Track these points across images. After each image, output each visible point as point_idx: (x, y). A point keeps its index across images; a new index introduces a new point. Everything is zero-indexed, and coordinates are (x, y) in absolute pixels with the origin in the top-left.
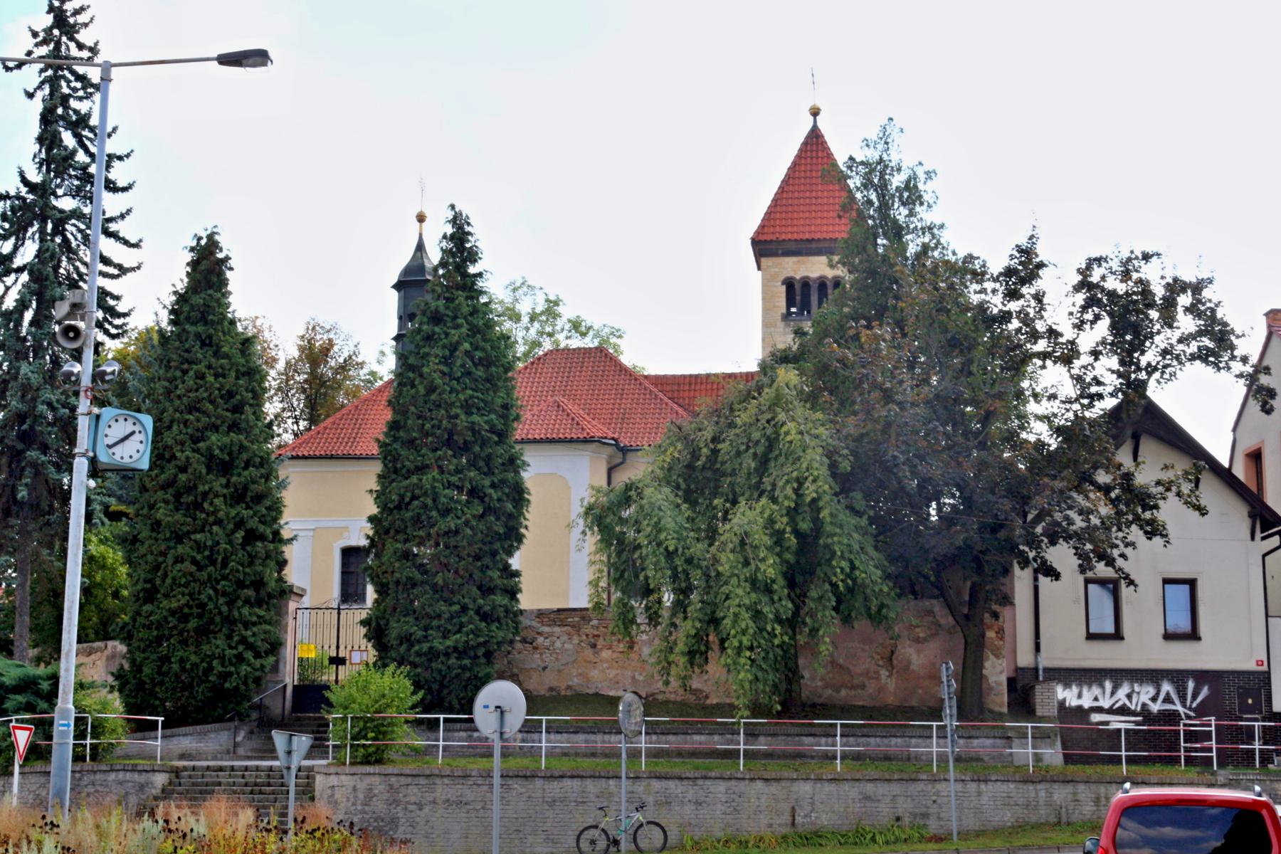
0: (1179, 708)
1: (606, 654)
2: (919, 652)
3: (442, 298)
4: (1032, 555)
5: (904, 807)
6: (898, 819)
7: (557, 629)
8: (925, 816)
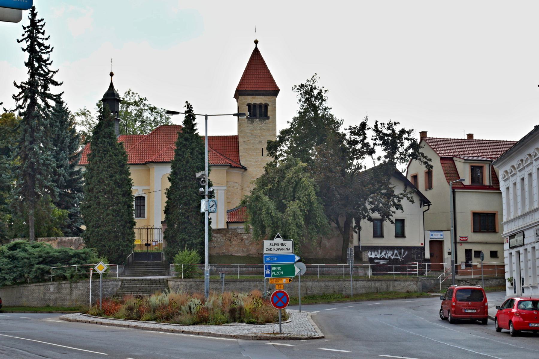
0: (399, 258)
1: (234, 243)
2: (328, 242)
3: (111, 99)
4: (366, 215)
5: (336, 288)
6: (335, 292)
7: (218, 235)
8: (342, 291)
